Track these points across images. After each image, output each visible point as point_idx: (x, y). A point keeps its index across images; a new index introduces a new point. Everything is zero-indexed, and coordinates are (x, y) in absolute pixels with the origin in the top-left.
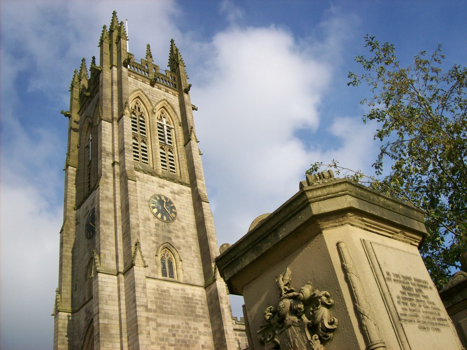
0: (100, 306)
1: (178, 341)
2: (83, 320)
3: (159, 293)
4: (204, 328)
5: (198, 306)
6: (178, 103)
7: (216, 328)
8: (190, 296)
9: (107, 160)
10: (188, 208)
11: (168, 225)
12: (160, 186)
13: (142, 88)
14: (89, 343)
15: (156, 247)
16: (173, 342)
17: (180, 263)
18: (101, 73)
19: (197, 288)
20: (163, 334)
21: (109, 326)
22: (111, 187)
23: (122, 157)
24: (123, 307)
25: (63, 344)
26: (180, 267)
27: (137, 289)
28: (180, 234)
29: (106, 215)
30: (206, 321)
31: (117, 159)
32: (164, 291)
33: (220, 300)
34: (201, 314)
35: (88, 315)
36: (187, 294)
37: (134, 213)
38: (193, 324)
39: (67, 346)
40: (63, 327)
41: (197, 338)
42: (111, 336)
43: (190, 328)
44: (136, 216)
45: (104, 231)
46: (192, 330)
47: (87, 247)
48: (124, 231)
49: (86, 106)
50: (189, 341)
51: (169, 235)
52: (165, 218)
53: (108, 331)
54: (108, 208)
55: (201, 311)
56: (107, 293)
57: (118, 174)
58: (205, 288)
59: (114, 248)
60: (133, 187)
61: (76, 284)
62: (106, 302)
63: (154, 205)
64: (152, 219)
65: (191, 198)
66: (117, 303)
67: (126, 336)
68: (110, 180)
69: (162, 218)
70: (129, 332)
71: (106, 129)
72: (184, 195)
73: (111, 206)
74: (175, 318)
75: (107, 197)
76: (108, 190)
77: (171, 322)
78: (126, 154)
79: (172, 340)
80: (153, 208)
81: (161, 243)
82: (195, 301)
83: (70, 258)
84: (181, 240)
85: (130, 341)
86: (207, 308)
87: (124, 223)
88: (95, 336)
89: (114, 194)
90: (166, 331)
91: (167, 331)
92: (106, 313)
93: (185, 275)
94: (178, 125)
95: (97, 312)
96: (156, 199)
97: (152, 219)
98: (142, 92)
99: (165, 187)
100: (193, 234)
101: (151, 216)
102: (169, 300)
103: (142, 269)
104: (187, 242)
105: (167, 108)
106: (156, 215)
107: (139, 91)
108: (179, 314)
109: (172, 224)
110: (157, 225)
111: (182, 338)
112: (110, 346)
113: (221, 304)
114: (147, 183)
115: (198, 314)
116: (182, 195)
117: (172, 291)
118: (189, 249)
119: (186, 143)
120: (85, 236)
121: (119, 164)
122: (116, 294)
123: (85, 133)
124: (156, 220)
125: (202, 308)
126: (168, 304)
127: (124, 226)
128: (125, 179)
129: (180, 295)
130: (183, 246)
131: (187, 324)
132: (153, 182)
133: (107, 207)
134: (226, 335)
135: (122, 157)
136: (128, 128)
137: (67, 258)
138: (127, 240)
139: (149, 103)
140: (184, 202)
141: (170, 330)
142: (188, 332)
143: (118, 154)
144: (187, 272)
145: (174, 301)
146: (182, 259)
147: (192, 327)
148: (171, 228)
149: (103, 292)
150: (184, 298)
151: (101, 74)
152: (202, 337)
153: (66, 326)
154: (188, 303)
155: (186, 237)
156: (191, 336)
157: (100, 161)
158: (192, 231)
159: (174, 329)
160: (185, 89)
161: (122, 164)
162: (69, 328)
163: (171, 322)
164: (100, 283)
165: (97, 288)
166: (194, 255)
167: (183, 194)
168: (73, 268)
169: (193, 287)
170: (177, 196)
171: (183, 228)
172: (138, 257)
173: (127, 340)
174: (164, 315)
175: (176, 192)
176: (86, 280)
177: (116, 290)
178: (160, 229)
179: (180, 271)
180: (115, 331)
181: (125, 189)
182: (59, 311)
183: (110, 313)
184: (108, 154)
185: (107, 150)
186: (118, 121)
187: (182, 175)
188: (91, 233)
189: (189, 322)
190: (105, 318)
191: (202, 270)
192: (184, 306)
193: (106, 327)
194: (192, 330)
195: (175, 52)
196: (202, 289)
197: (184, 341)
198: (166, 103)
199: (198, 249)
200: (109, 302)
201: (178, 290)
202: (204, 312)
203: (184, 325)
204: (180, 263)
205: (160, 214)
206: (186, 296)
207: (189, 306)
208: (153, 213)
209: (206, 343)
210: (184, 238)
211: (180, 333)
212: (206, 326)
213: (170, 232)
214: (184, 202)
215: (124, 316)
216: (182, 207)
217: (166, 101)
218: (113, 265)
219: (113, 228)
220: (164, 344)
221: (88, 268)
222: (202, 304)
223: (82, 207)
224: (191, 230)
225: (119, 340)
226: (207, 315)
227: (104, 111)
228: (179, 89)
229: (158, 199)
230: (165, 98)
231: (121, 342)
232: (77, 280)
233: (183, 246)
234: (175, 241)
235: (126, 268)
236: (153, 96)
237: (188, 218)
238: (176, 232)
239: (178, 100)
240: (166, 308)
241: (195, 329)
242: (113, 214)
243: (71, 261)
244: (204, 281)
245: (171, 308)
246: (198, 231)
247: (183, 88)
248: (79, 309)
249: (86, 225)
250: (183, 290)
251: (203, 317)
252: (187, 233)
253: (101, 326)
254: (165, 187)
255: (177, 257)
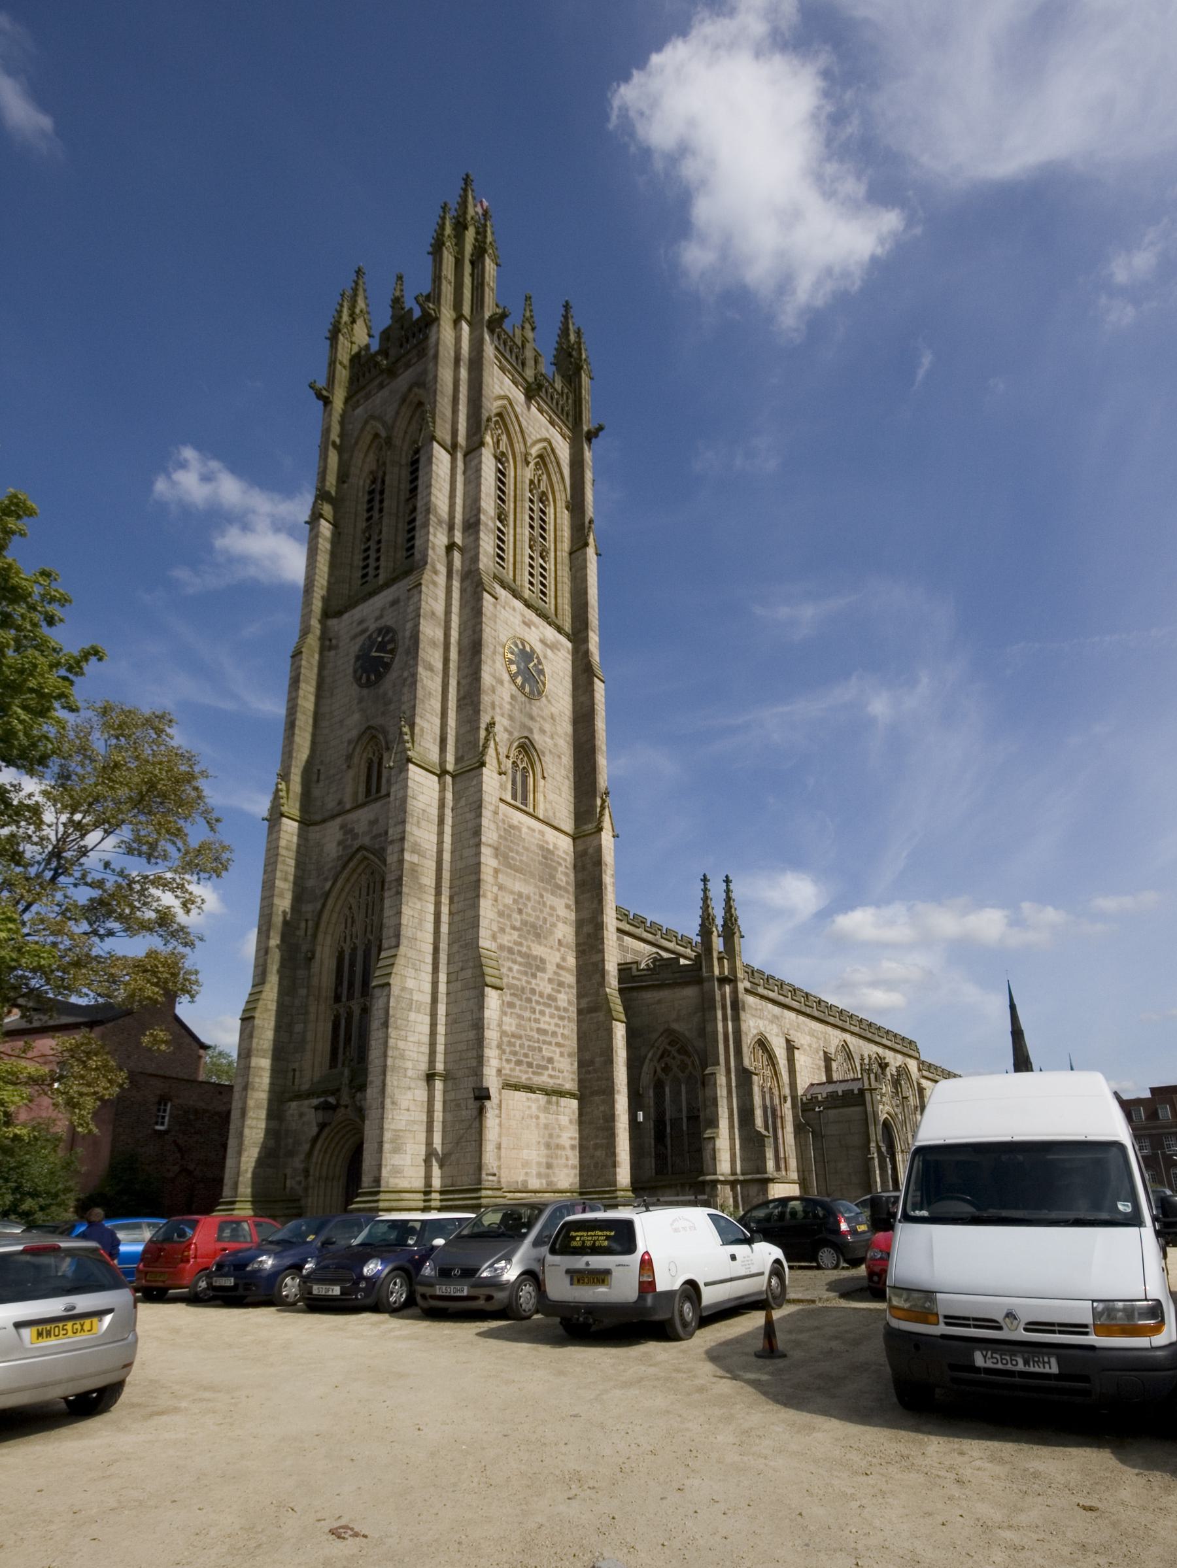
0: (408, 828)
1: (524, 923)
2: (334, 844)
3: (505, 829)
4: (565, 910)
5: (560, 869)
6: (568, 457)
7: (586, 914)
8: (551, 847)
9: (439, 535)
10: (564, 682)
11: (530, 703)
12: (524, 623)
13: (511, 396)
14: (342, 890)
15: (509, 739)
16: (518, 924)
17: (542, 782)
18: (436, 324)
19: (562, 836)
20: (505, 906)
21: (419, 869)
22: (441, 594)
23: (472, 538)
24: (448, 839)
25: (286, 880)
26: (540, 788)
27: (484, 812)
28: (547, 727)
29: (430, 651)
30: (568, 899)
31: (458, 538)
32: (512, 827)
33: (603, 867)
34: (563, 884)
35: (349, 836)
36: (547, 843)
37: (489, 662)
38: (550, 900)
39: (291, 885)
40: (287, 849)
41: (554, 925)
42: (421, 887)
43: (544, 904)
44: (492, 671)
45: (425, 682)
46: (547, 910)
47: (356, 702)
48: (462, 692)
49: (370, 391)
50: (541, 926)
51: (530, 724)
52: (527, 689)
53: (417, 878)
54: (434, 637)
55: (564, 879)
56: (421, 806)
57: (457, 571)
58: (574, 839)
59: (437, 721)
60: (491, 608)
61: (319, 770)
62: (418, 822)
63: (513, 657)
64: (506, 684)
65: (570, 662)
66: (435, 828)
67: (448, 894)
68: (441, 580)
69: (523, 687)
70: (457, 889)
71: (440, 465)
72: (559, 654)
73: (439, 634)
74: (525, 880)
75: (433, 614)
76: (436, 600)
77: (519, 886)
78: (482, 535)
79: (516, 920)
80: (511, 662)
81: (516, 734)
82: (556, 858)
83: (311, 714)
84: (548, 740)
85: (455, 905)
86: (572, 876)
87: (465, 677)
88: (391, 882)
89: (448, 612)
90: (509, 900)
91: (511, 902)
92: (416, 844)
93: (548, 806)
94: (564, 505)
95: (399, 836)
96: (516, 646)
97: (506, 684)
98: (511, 404)
99: (533, 628)
100: (566, 734)
101: (506, 677)
102: (518, 845)
103: (496, 776)
104: (556, 745)
105: (547, 459)
106: (513, 678)
107: (506, 402)
108: (532, 875)
109: (537, 703)
110: (513, 697)
111: (532, 920)
112: (418, 906)
113: (604, 876)
114: (504, 608)
115: (560, 882)
116: (556, 651)
117: (524, 830)
118: (557, 760)
119: (575, 548)
120: (350, 678)
121: (461, 550)
122: (434, 811)
123: (361, 455)
124: (513, 687)
125: (566, 875)
126: (517, 852)
127: (463, 682)
128: (477, 586)
129: (536, 842)
130: (550, 751)
131: (542, 896)
132: (514, 609)
133: (432, 634)
134: (605, 932)
135: (472, 538)
136: (488, 478)
137: (304, 713)
138: (471, 712)
139: (519, 435)
140: (559, 666)
141: (514, 900)
142: (541, 911)
143: (461, 530)
144: (551, 803)
145: (527, 849)
146: (546, 775)
147: (548, 903)
148: (535, 711)
149: (415, 802)
150: (542, 848)
151: (434, 329)
152: (560, 925)
153: (294, 847)
154: (546, 858)
155: (555, 737)
156: (545, 920)
157: (423, 532)
158: (565, 727)
159: (521, 900)
160: (589, 432)
161: (471, 553)
162: (298, 852)
163: (519, 886)
164: (410, 783)
165: (402, 791)
166: (563, 772)
167: (559, 650)
168: (314, 736)
169: (556, 833)
170: (549, 652)
171: (553, 717)
172: (491, 751)
173: (448, 902)
174: (509, 870)
175: (549, 642)
176: (349, 767)
177: (436, 804)
178: (517, 707)
179: (540, 797)
180: (429, 880)
181: (473, 609)
182: (282, 815)
183: (422, 845)
184: (440, 522)
185: (439, 511)
186: (465, 455)
187: (560, 612)
188: (373, 677)
189: (544, 894)
190: (413, 852)
191: (572, 806)
192: (540, 863)
193: (414, 868)
194: (547, 910)
195: (572, 338)
196: (569, 840)
197: (534, 926)
198: (549, 449)
199: (571, 763)
200: (423, 823)
201: (533, 830)
202: (567, 883)
203: (537, 897)
204: (542, 782)
205: (520, 678)
206: (546, 846)
207: (547, 865)
208: (509, 672)
209: (564, 937)
210: (552, 738)
211: (530, 911)
212: (567, 907)
213: (532, 718)
214: (559, 666)
215: (447, 856)
216: (555, 675)
217: (550, 443)
218: (434, 755)
219: (439, 680)
220: (505, 924)
221: (357, 742)
222: (566, 867)
223: (346, 616)
224: (564, 724)
225: (432, 899)
226: (571, 889)
227: (438, 420)
228: (573, 427)
229: (521, 647)
230: (548, 436)
231: (438, 904)
232: (322, 763)
233: (550, 751)
234: (537, 737)
235: (459, 766)
236: (528, 424)
237: (561, 700)
238: (542, 722)
239: (568, 451)
240: (513, 858)
241: (552, 908)
242: (441, 650)
243: (311, 721)
244: (573, 827)
245: (521, 861)
246: (575, 731)
247: (585, 428)
248: (324, 821)
249: (358, 658)
250: (542, 833)
251: (567, 891)
252: (559, 728)
253: (406, 866)
254: (533, 628)
255: (538, 769)
